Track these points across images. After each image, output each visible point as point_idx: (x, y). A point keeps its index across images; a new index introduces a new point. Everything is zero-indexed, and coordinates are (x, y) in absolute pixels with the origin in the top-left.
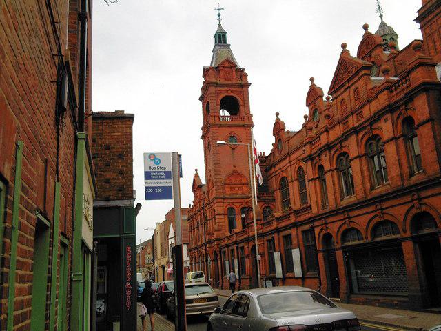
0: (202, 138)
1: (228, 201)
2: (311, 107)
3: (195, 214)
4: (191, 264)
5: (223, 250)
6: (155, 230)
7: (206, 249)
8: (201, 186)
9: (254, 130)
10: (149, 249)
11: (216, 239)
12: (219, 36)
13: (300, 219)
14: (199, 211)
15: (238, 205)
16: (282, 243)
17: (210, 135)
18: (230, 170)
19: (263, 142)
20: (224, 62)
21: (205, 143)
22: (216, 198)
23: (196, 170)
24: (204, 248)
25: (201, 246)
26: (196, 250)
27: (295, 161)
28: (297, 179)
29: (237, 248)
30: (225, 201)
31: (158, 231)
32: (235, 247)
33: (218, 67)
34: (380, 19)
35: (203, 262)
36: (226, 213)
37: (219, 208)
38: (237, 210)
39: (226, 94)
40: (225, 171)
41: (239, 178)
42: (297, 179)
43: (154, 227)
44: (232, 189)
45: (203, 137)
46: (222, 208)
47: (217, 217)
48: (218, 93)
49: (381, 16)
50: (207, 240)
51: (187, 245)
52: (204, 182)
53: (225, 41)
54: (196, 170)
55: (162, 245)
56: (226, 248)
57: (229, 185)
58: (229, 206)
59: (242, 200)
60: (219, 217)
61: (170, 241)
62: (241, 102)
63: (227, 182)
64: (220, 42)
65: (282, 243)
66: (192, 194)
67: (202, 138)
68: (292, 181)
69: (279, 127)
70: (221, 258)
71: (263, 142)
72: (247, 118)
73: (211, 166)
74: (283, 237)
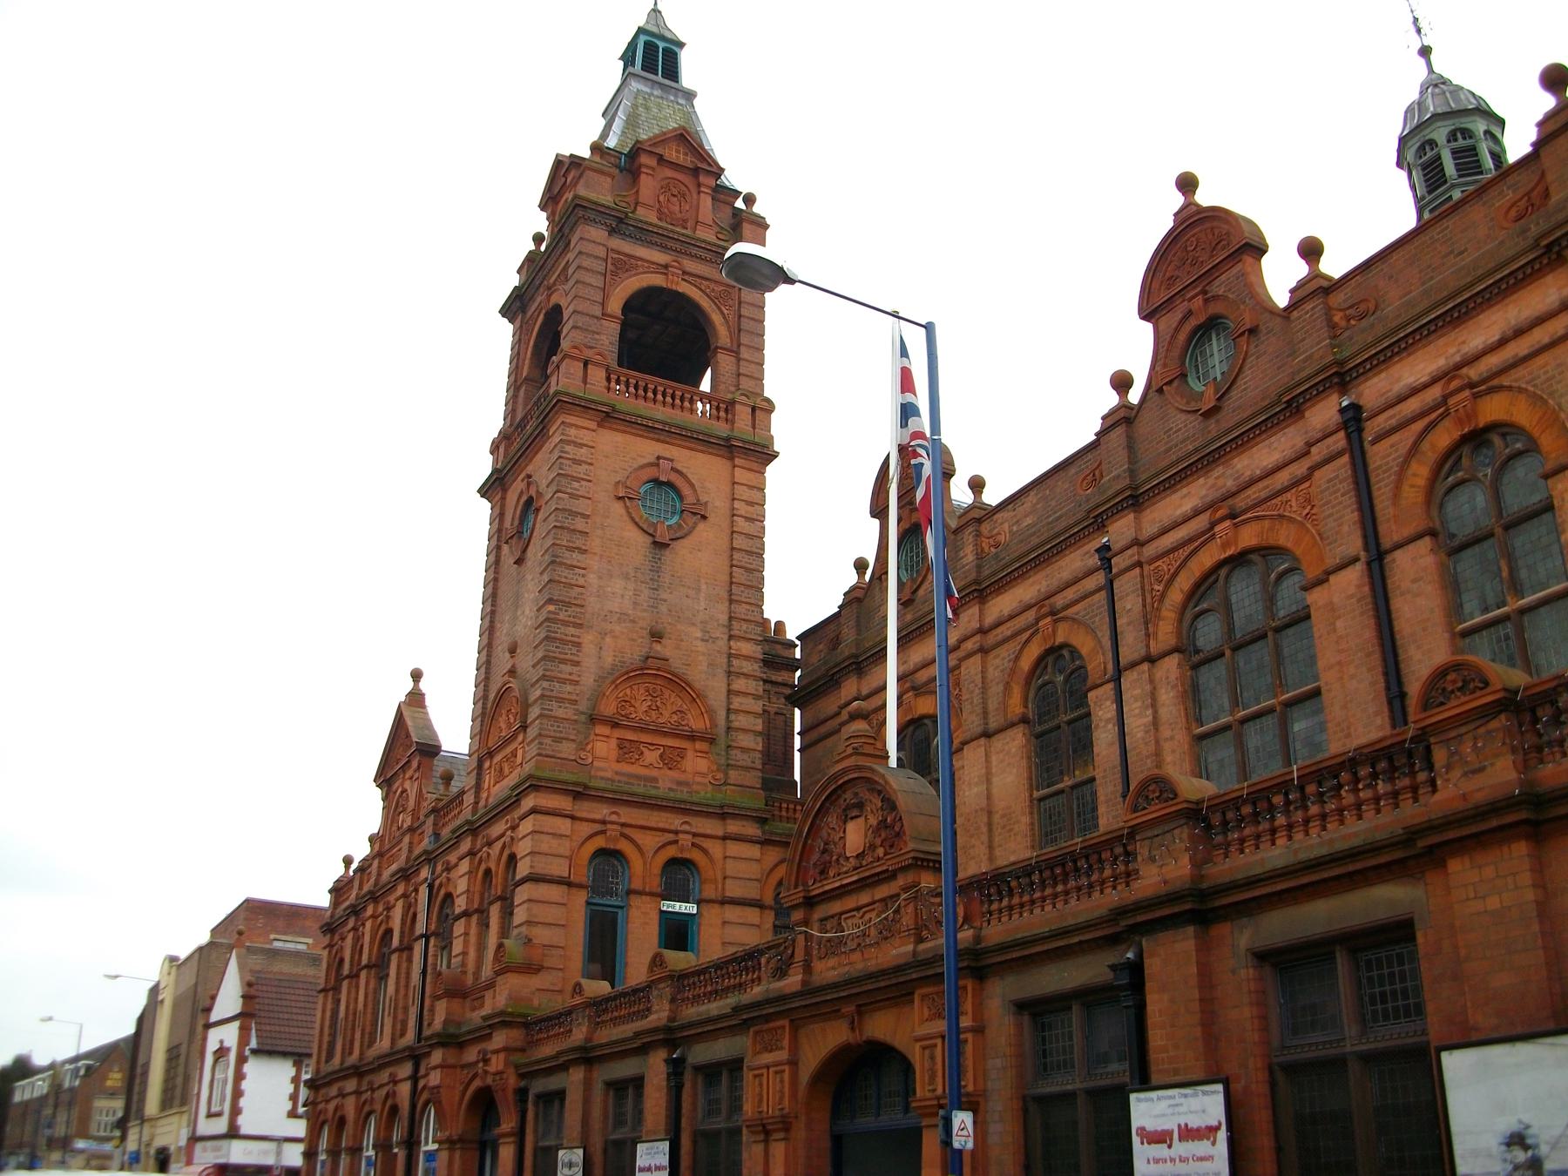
0: (485, 491)
1: (602, 811)
2: (1171, 319)
3: (373, 897)
4: (310, 1155)
5: (539, 1086)
6: (154, 991)
7: (415, 1078)
8: (431, 750)
9: (779, 481)
10: (115, 1078)
11: (503, 1020)
12: (650, 48)
13: (692, 1012)
14: (405, 874)
15: (649, 841)
16: (596, 1112)
17: (541, 468)
18: (634, 652)
19: (813, 552)
20: (663, 139)
21: (498, 518)
22: (533, 784)
23: (417, 675)
24: (405, 1070)
25: (390, 1060)
26: (351, 1085)
27: (1030, 616)
28: (1024, 720)
29: (676, 1068)
30: (586, 809)
31: (167, 996)
32: (655, 1068)
33: (636, 151)
34: (1422, 61)
35: (383, 1146)
36: (583, 874)
37: (545, 841)
38: (643, 867)
39: (658, 280)
40: (601, 651)
41: (673, 701)
42: (1024, 720)
43: (153, 972)
44: (627, 750)
45: (492, 488)
46: (564, 847)
47: (522, 894)
48: (621, 265)
49: (1425, 52)
50: (1425, 653)
51: (298, 1064)
52: (454, 730)
53: (672, 71)
54: (417, 675)
55: (173, 1055)
56: (577, 1075)
57: (615, 725)
58: (599, 842)
59: (676, 822)
60: (543, 891)
61: (214, 1038)
62: (723, 335)
63: (609, 708)
64: (649, 66)
65: (596, 1112)
66: (377, 793)
67: (485, 491)
68: (1151, 659)
69: (911, 487)
70: (520, 1134)
71: (813, 552)
72: (743, 413)
73: (524, 621)
74: (609, 1084)
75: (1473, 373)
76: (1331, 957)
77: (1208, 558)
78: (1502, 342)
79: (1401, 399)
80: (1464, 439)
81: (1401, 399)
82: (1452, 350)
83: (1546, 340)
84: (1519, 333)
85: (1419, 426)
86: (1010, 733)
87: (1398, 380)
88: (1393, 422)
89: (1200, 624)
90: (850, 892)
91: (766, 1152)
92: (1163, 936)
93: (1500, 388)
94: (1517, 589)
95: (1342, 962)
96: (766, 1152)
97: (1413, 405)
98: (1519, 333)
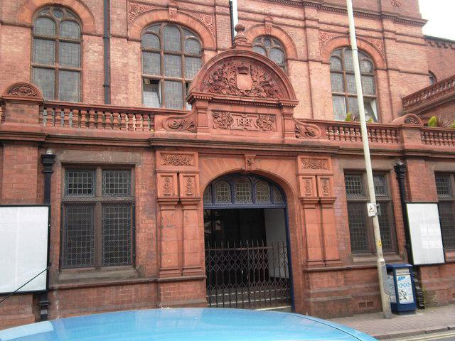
75: (276, 19)
76: (95, 170)
77: (162, 16)
78: (282, 17)
79: (249, 12)
80: (263, 36)
81: (249, 12)
82: (266, 9)
83: (293, 24)
84: (287, 18)
85: (154, 8)
86: (23, 30)
87: (248, 5)
88: (244, 17)
89: (47, 21)
90: (242, 105)
91: (324, 253)
92: (415, 161)
93: (279, 28)
94: (57, 61)
95: (99, 171)
96: (324, 253)
97: (251, 16)
98: (287, 18)
